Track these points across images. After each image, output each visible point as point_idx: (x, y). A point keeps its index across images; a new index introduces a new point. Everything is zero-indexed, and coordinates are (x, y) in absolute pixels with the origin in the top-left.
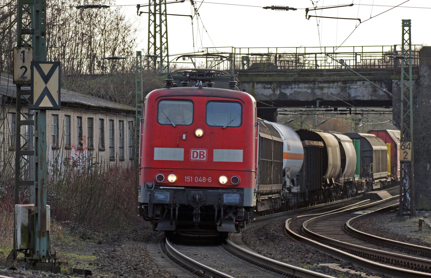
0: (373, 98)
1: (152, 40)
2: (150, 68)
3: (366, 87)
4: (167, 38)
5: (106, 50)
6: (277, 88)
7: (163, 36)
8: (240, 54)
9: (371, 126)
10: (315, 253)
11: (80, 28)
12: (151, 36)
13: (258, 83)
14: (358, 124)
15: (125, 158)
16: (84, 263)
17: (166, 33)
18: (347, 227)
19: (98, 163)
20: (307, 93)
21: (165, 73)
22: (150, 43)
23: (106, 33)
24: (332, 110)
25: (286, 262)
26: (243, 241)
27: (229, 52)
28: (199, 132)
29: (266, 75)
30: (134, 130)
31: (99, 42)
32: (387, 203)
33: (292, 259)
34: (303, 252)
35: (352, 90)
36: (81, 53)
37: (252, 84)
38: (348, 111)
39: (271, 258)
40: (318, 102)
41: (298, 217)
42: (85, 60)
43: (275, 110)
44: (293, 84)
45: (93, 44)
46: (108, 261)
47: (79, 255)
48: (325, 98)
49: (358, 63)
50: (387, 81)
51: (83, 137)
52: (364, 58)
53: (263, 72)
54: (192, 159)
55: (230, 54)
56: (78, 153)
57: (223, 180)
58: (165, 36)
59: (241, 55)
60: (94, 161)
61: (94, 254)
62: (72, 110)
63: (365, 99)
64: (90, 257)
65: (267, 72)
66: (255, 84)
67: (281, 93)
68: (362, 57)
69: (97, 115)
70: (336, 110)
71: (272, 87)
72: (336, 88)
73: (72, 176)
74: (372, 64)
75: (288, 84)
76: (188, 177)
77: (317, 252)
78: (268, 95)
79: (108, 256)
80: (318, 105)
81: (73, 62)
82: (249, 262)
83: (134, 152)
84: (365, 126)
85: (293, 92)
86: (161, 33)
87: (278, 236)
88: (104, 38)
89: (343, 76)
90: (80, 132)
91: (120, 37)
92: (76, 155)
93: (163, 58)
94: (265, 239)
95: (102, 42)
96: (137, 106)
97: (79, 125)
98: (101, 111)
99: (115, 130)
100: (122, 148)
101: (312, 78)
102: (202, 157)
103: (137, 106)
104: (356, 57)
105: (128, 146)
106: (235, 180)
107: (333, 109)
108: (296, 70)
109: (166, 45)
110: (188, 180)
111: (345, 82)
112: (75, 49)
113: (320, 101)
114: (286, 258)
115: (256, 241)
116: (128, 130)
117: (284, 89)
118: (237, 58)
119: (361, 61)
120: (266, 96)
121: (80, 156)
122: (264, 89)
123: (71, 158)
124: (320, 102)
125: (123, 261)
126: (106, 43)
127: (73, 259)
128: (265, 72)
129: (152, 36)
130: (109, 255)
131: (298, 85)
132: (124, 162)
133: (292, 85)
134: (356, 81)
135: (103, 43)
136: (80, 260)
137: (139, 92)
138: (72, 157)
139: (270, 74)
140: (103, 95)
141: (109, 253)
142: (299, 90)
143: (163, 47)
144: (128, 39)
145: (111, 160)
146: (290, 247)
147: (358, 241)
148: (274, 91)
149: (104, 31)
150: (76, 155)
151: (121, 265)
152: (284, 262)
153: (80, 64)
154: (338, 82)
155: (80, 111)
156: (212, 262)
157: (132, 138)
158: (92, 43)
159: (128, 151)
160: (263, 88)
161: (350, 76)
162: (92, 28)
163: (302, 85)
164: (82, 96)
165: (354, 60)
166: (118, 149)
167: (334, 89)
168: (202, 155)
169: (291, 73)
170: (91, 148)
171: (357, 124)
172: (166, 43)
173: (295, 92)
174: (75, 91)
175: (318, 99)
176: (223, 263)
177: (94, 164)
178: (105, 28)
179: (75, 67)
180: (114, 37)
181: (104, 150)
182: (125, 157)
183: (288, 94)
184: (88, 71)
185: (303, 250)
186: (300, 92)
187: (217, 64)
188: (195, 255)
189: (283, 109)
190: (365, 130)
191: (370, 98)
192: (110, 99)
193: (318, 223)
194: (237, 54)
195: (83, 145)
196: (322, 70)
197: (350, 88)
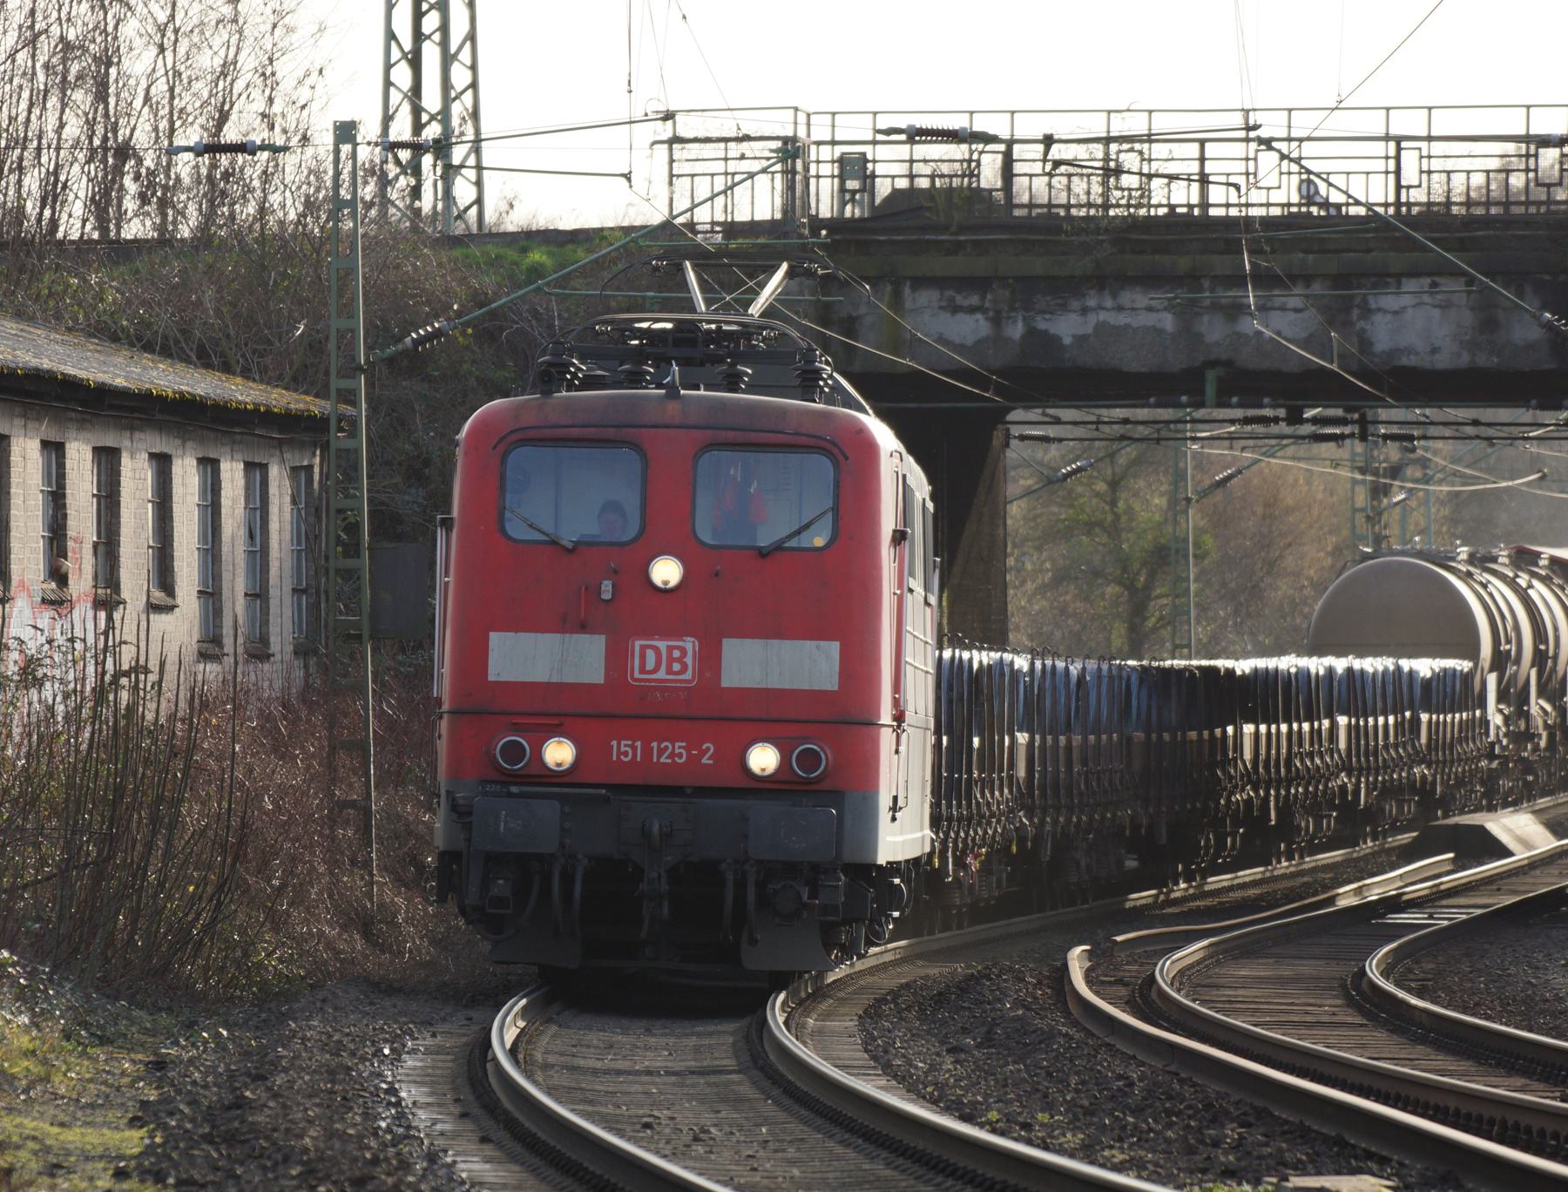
0: (1483, 360)
1: (402, 75)
2: (392, 210)
3: (1445, 306)
4: (473, 67)
5: (178, 124)
6: (1012, 309)
7: (455, 57)
8: (833, 143)
9: (1443, 503)
10: (1251, 1119)
11: (55, 15)
12: (396, 54)
13: (919, 282)
14: (1386, 495)
15: (275, 645)
16: (89, 1166)
17: (468, 44)
18: (1371, 983)
19: (147, 671)
20: (1159, 332)
21: (470, 236)
22: (392, 89)
23: (176, 40)
24: (1276, 420)
25: (1117, 1168)
26: (874, 1058)
27: (782, 133)
28: (666, 571)
29: (957, 247)
30: (317, 510)
31: (144, 84)
32: (1538, 872)
33: (1142, 1153)
34: (1190, 1117)
35: (1378, 318)
36: (59, 139)
37: (889, 288)
38: (1353, 422)
39: (1029, 1142)
40: (1211, 376)
41: (1119, 938)
42: (76, 168)
43: (997, 416)
44: (1092, 292)
45: (118, 95)
46: (208, 1156)
47: (62, 1125)
48: (1248, 359)
49: (1409, 187)
50: (1547, 277)
51: (70, 544)
52: (1436, 164)
53: (944, 229)
54: (637, 675)
55: (785, 140)
56: (44, 622)
57: (763, 759)
58: (395, 97)
59: (839, 150)
60: (127, 656)
61: (135, 1122)
62: (18, 410)
63: (1443, 362)
64: (118, 1136)
65: (962, 229)
66: (907, 291)
67: (1031, 333)
68: (1429, 157)
69: (137, 435)
70: (1295, 418)
71: (987, 305)
72: (1297, 310)
73: (16, 731)
74: (1473, 194)
75: (1065, 289)
76: (623, 743)
77: (1261, 1114)
78: (969, 341)
79: (210, 1134)
80: (1210, 390)
81: (19, 182)
82: (927, 1164)
83: (318, 619)
84: (1413, 503)
85: (1089, 330)
86: (444, 43)
87: (1051, 1035)
88: (169, 66)
89: (1336, 251)
90: (55, 517)
91: (248, 62)
92: (35, 627)
93: (472, 161)
94: (979, 1046)
95: (161, 87)
96: (333, 394)
97: (50, 485)
98: (158, 416)
99: (223, 511)
100: (256, 596)
101: (1184, 263)
102: (676, 667)
103: (333, 394)
104: (1398, 158)
105: (287, 588)
106: (809, 758)
107: (1282, 413)
108: (1104, 223)
109: (468, 98)
110: (626, 754)
111: (1342, 280)
112: (28, 120)
113: (1220, 371)
114: (1111, 1147)
115: (938, 1054)
116: (288, 507)
117: (1044, 312)
118: (818, 162)
119: (1425, 176)
120: (960, 348)
121: (58, 631)
122: (949, 315)
123: (13, 644)
124: (1219, 379)
125: (286, 1159)
126: (177, 90)
127: (31, 1144)
128: (953, 229)
129: (405, 55)
130: (213, 1127)
131: (1114, 296)
132: (266, 667)
133: (1084, 296)
134: (1398, 277)
135: (166, 88)
136: (68, 1153)
137: (343, 323)
138: (18, 639)
139: (976, 243)
140: (165, 337)
141: (209, 1116)
142: (1122, 319)
143: (457, 109)
144: (286, 70)
145: (203, 656)
146: (1119, 1090)
147: (1452, 1064)
148: (997, 321)
149: (170, 34)
150: (35, 627)
151: (276, 1178)
152: (1103, 1166)
153: (53, 193)
154: (1308, 280)
155: (59, 418)
156: (738, 1163)
157: (309, 550)
158: (112, 90)
159: (288, 613)
160: (941, 308)
161: (1368, 251)
162: (110, 16)
163: (1136, 297)
164: (63, 343)
165: (1387, 172)
166: (241, 602)
167: (1292, 316)
168: (677, 660)
169: (1083, 238)
170: (108, 600)
171: (1379, 491)
172: (470, 91)
173: (1100, 327)
174: (31, 319)
175: (1213, 364)
176: (796, 1172)
177: (127, 674)
178: (172, 17)
179: (31, 207)
180: (218, 61)
181: (170, 609)
182: (272, 639)
183: (1067, 341)
184: (88, 226)
185: (1189, 1107)
186: (1127, 326)
187: (722, 188)
188: (647, 1126)
189: (1047, 415)
190: (1416, 524)
191: (1465, 360)
192: (199, 358)
193: (1223, 971)
194: (819, 143)
195: (70, 582)
196: (1227, 222)
197: (1367, 312)
